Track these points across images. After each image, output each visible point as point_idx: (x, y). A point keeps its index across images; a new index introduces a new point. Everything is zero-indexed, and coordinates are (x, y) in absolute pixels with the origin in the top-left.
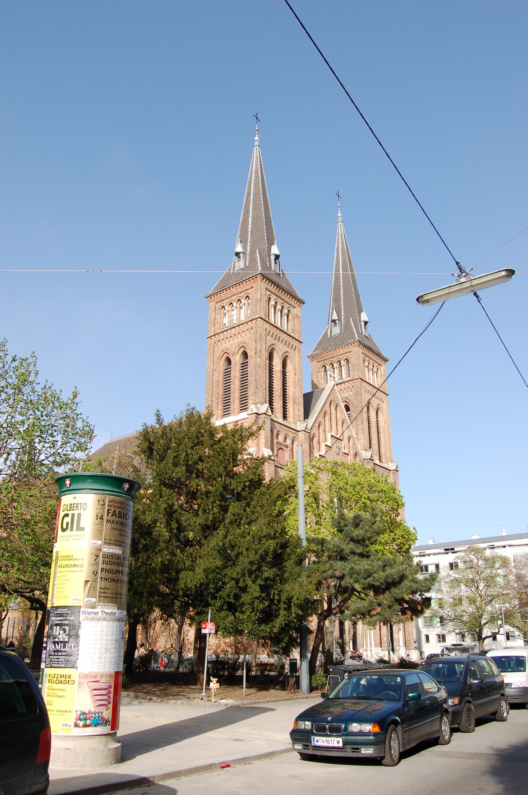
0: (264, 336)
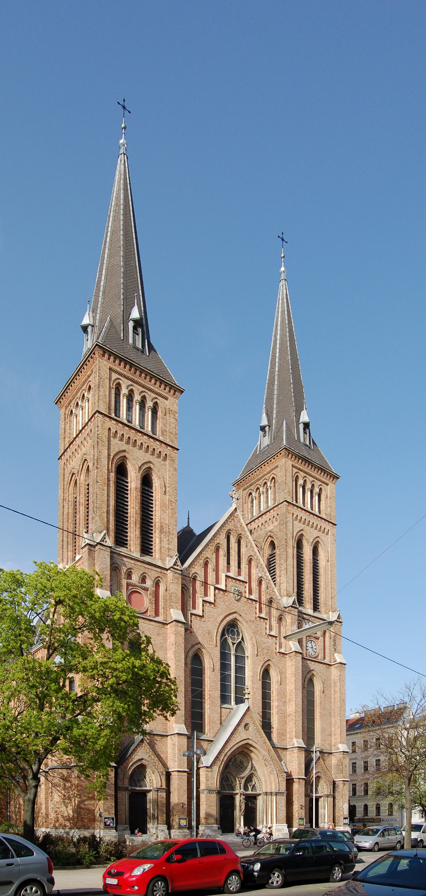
0: (105, 439)
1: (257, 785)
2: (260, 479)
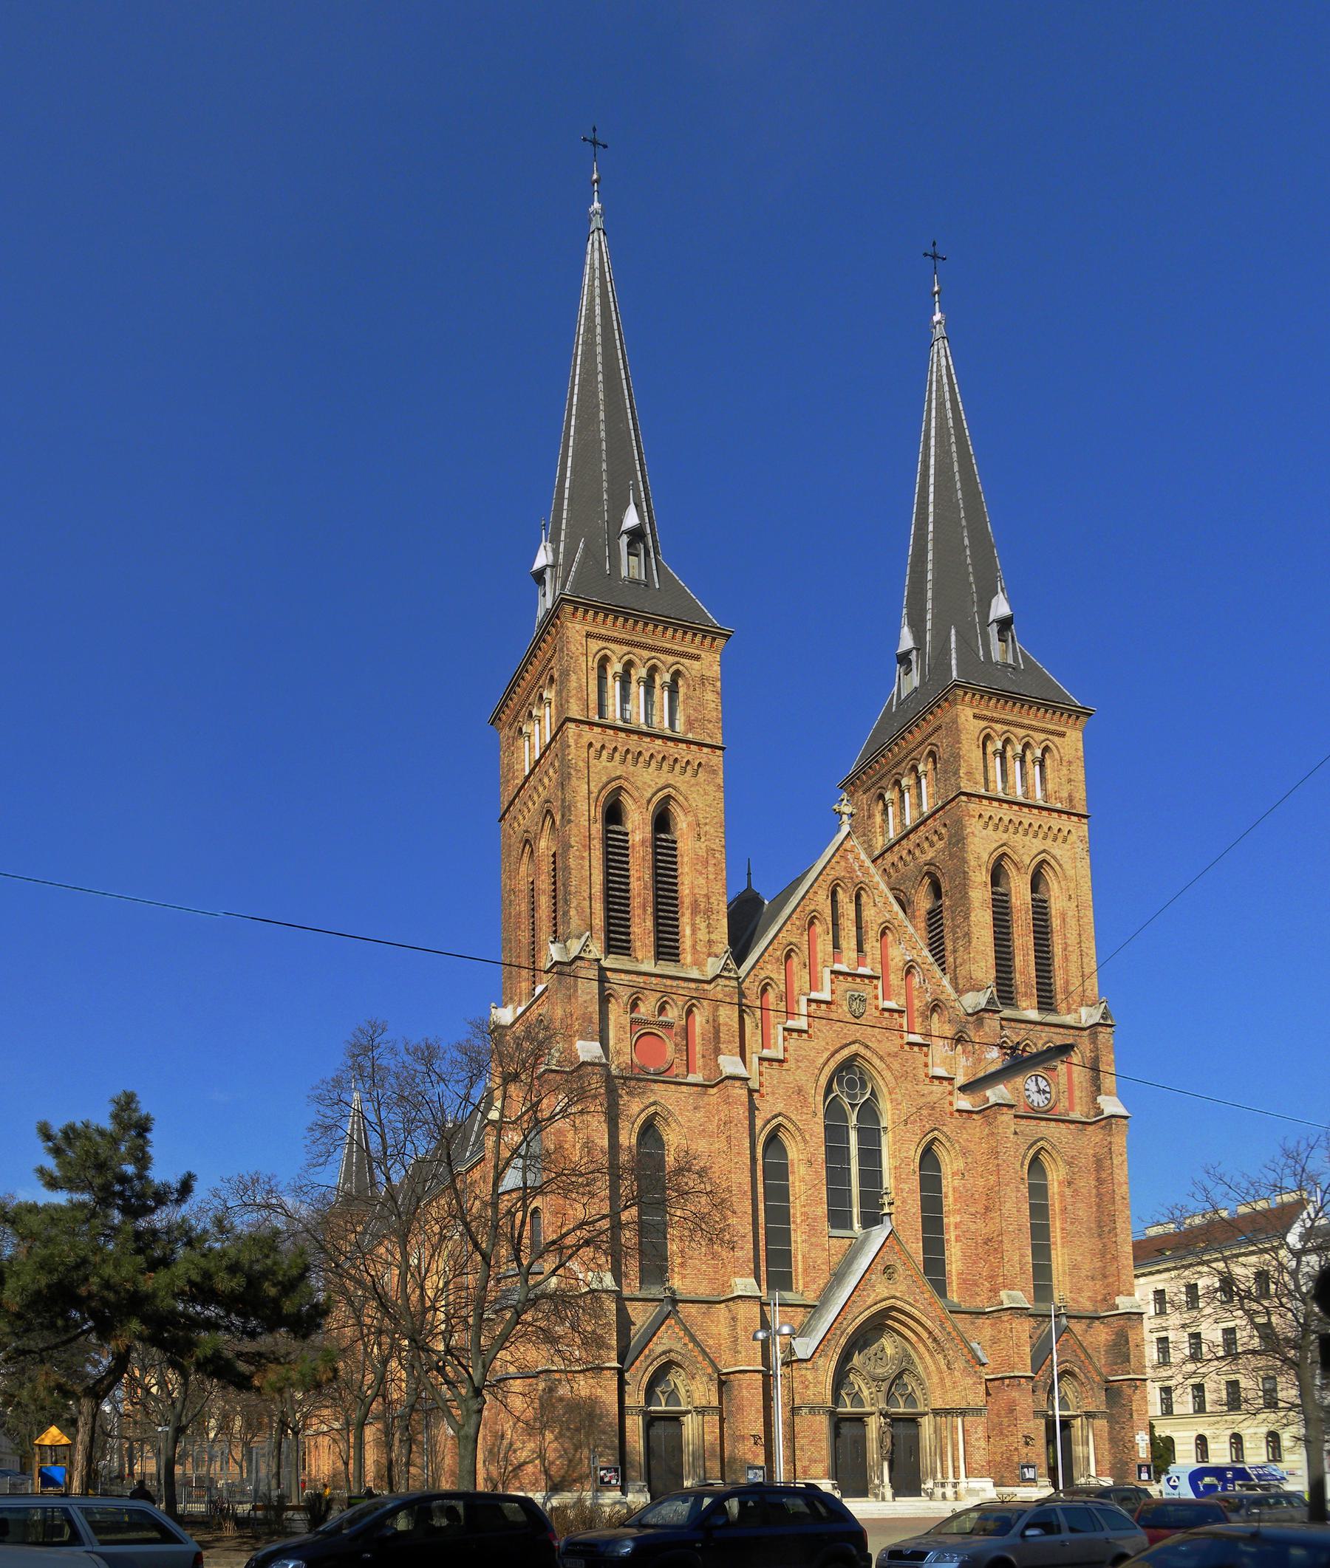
1: (918, 1393)
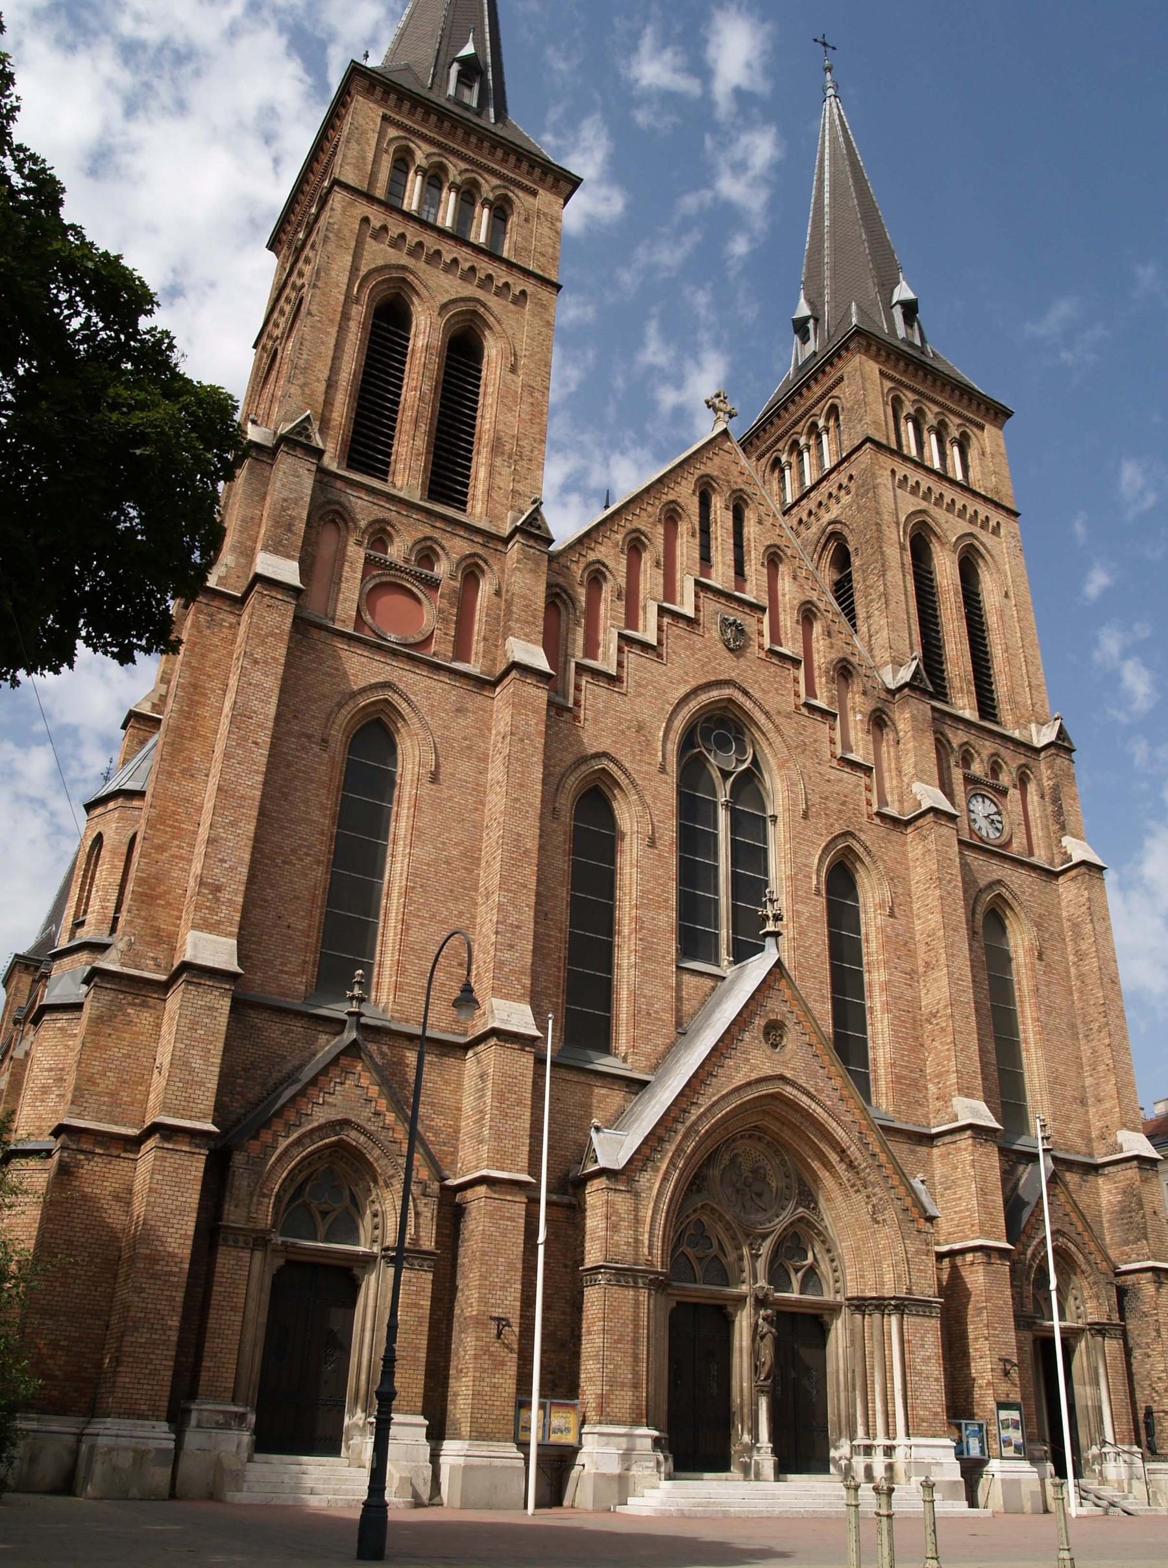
1: (825, 1268)
2: (800, 421)
